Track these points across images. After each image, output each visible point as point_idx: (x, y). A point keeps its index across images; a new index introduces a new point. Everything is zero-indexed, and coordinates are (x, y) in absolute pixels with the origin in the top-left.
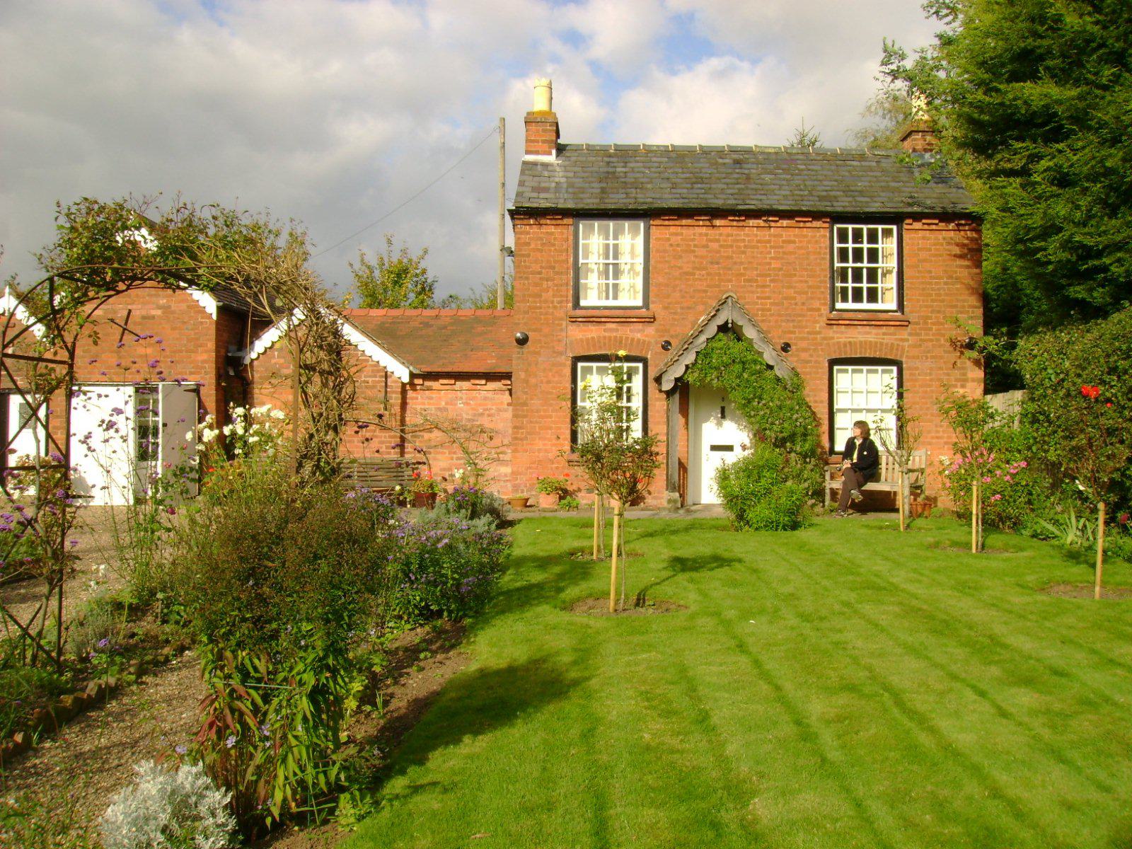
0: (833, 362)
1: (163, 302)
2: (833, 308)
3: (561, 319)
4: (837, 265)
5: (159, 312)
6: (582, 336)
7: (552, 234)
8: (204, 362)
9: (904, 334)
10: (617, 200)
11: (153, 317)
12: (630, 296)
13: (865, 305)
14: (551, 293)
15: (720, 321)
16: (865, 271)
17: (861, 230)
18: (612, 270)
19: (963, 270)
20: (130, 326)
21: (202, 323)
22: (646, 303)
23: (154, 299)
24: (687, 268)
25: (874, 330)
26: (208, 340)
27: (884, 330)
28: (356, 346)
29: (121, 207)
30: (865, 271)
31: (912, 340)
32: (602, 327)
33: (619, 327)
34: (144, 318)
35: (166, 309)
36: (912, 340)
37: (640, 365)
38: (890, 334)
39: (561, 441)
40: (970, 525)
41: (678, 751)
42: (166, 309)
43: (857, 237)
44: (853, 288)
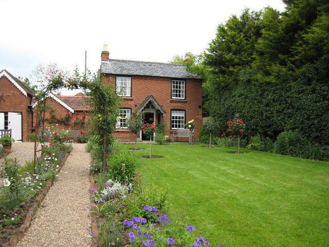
0: (171, 110)
1: (12, 92)
2: (171, 98)
4: (173, 89)
5: (11, 94)
6: (131, 104)
10: (125, 72)
11: (9, 96)
12: (128, 95)
13: (178, 98)
15: (149, 100)
18: (123, 89)
19: (74, 90)
20: (3, 98)
22: (131, 96)
24: (141, 88)
29: (220, 27)
31: (188, 106)
34: (7, 96)
35: (13, 93)
36: (188, 106)
41: (216, 188)
43: (177, 83)
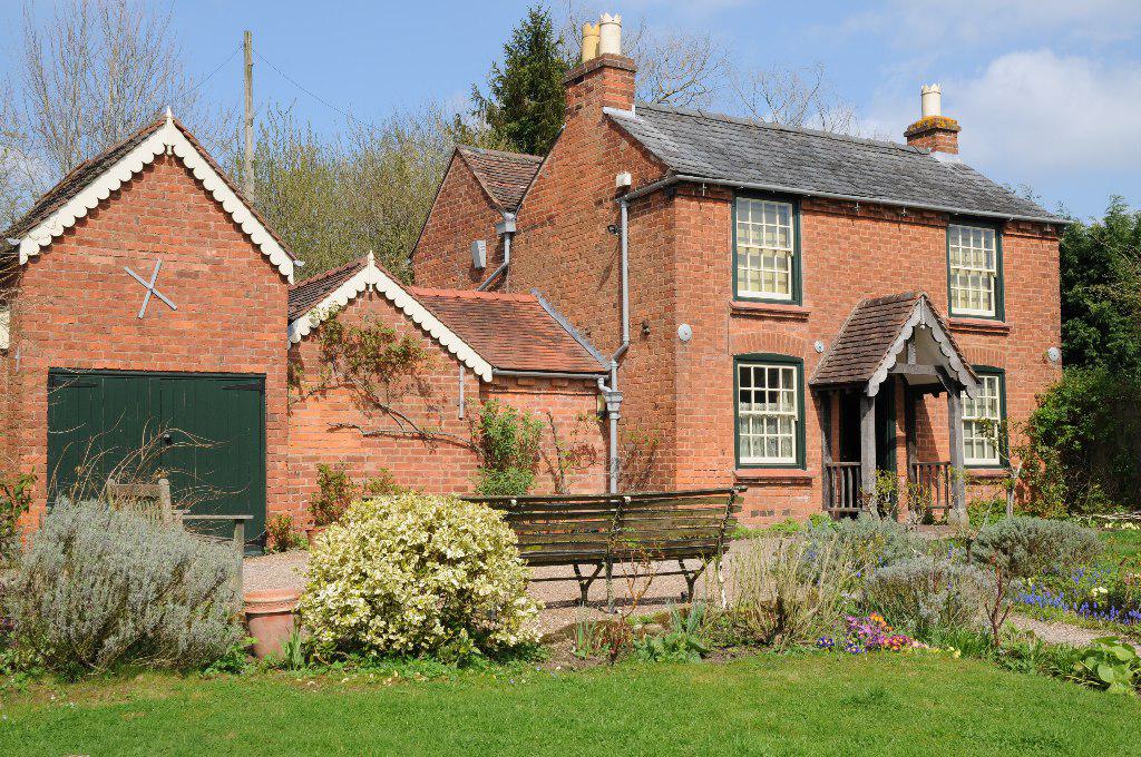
3: (723, 311)
5: (206, 268)
7: (712, 209)
8: (273, 345)
9: (1004, 341)
11: (196, 275)
14: (711, 281)
16: (780, 372)
17: (763, 370)
21: (269, 288)
23: (195, 248)
25: (984, 338)
26: (278, 313)
27: (990, 337)
28: (100, 201)
30: (780, 372)
32: (761, 323)
33: (776, 324)
35: (216, 264)
37: (795, 369)
38: (995, 342)
39: (726, 457)
40: (776, 426)
42: (216, 264)
44: (750, 392)
